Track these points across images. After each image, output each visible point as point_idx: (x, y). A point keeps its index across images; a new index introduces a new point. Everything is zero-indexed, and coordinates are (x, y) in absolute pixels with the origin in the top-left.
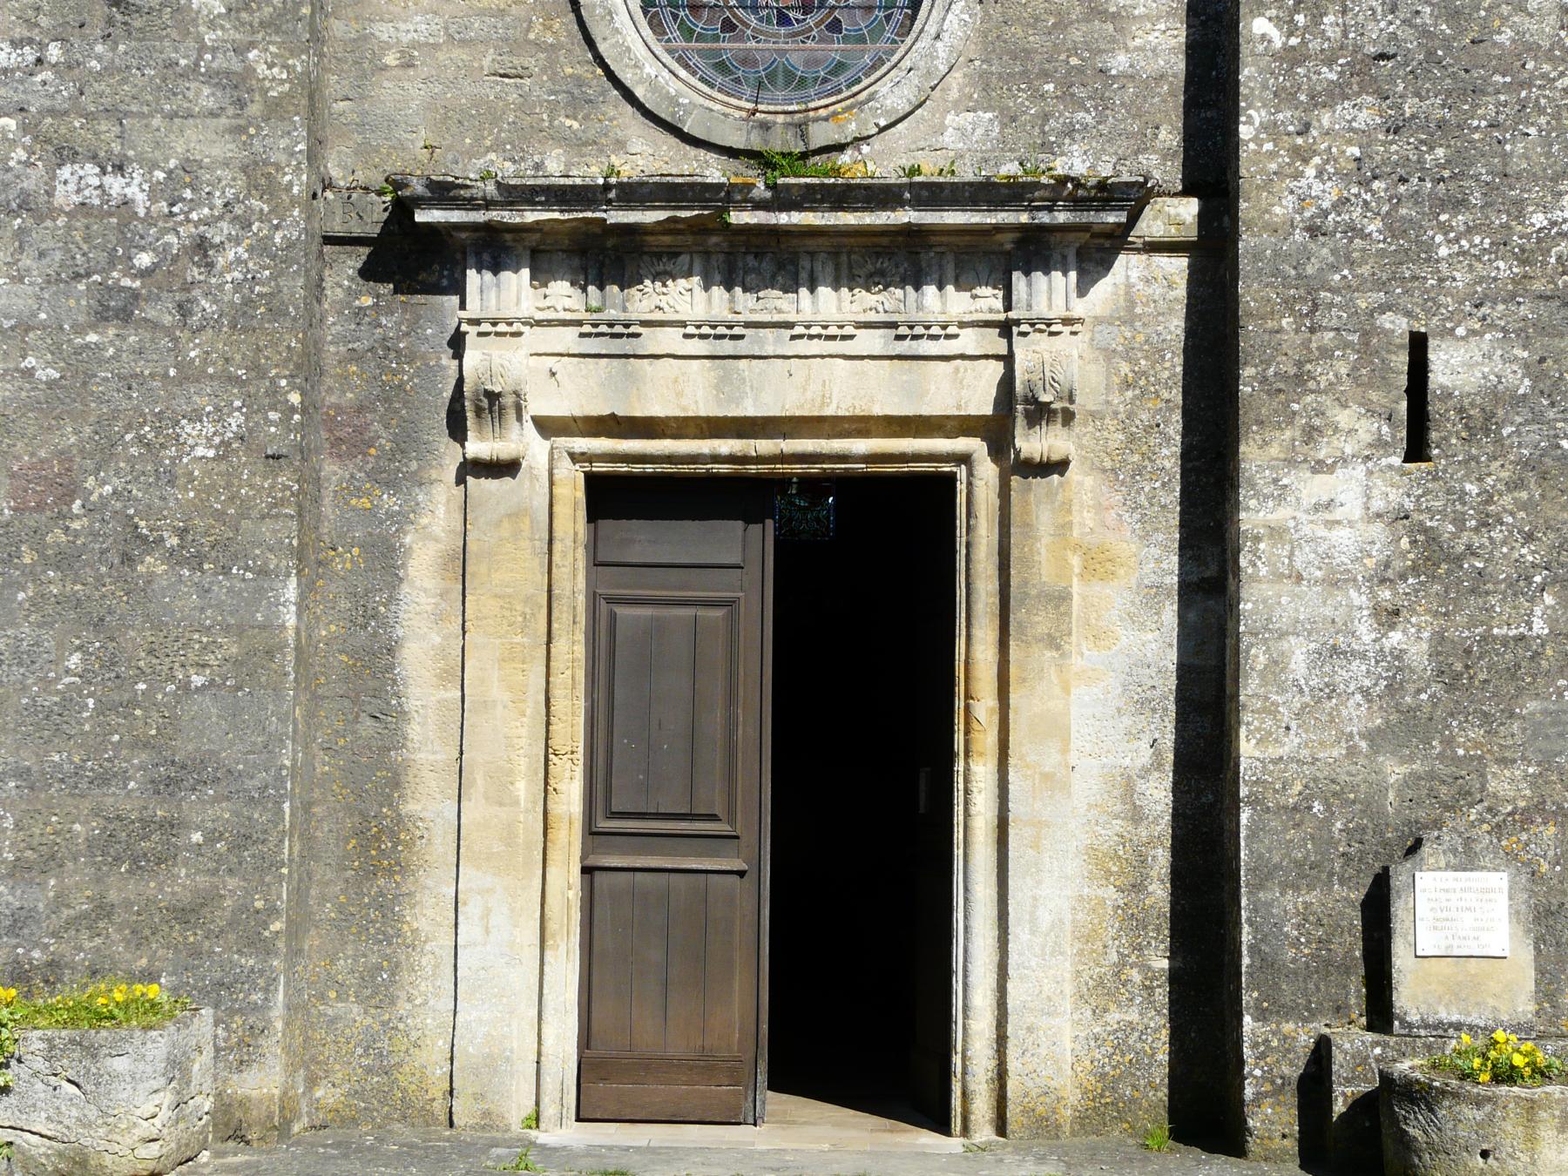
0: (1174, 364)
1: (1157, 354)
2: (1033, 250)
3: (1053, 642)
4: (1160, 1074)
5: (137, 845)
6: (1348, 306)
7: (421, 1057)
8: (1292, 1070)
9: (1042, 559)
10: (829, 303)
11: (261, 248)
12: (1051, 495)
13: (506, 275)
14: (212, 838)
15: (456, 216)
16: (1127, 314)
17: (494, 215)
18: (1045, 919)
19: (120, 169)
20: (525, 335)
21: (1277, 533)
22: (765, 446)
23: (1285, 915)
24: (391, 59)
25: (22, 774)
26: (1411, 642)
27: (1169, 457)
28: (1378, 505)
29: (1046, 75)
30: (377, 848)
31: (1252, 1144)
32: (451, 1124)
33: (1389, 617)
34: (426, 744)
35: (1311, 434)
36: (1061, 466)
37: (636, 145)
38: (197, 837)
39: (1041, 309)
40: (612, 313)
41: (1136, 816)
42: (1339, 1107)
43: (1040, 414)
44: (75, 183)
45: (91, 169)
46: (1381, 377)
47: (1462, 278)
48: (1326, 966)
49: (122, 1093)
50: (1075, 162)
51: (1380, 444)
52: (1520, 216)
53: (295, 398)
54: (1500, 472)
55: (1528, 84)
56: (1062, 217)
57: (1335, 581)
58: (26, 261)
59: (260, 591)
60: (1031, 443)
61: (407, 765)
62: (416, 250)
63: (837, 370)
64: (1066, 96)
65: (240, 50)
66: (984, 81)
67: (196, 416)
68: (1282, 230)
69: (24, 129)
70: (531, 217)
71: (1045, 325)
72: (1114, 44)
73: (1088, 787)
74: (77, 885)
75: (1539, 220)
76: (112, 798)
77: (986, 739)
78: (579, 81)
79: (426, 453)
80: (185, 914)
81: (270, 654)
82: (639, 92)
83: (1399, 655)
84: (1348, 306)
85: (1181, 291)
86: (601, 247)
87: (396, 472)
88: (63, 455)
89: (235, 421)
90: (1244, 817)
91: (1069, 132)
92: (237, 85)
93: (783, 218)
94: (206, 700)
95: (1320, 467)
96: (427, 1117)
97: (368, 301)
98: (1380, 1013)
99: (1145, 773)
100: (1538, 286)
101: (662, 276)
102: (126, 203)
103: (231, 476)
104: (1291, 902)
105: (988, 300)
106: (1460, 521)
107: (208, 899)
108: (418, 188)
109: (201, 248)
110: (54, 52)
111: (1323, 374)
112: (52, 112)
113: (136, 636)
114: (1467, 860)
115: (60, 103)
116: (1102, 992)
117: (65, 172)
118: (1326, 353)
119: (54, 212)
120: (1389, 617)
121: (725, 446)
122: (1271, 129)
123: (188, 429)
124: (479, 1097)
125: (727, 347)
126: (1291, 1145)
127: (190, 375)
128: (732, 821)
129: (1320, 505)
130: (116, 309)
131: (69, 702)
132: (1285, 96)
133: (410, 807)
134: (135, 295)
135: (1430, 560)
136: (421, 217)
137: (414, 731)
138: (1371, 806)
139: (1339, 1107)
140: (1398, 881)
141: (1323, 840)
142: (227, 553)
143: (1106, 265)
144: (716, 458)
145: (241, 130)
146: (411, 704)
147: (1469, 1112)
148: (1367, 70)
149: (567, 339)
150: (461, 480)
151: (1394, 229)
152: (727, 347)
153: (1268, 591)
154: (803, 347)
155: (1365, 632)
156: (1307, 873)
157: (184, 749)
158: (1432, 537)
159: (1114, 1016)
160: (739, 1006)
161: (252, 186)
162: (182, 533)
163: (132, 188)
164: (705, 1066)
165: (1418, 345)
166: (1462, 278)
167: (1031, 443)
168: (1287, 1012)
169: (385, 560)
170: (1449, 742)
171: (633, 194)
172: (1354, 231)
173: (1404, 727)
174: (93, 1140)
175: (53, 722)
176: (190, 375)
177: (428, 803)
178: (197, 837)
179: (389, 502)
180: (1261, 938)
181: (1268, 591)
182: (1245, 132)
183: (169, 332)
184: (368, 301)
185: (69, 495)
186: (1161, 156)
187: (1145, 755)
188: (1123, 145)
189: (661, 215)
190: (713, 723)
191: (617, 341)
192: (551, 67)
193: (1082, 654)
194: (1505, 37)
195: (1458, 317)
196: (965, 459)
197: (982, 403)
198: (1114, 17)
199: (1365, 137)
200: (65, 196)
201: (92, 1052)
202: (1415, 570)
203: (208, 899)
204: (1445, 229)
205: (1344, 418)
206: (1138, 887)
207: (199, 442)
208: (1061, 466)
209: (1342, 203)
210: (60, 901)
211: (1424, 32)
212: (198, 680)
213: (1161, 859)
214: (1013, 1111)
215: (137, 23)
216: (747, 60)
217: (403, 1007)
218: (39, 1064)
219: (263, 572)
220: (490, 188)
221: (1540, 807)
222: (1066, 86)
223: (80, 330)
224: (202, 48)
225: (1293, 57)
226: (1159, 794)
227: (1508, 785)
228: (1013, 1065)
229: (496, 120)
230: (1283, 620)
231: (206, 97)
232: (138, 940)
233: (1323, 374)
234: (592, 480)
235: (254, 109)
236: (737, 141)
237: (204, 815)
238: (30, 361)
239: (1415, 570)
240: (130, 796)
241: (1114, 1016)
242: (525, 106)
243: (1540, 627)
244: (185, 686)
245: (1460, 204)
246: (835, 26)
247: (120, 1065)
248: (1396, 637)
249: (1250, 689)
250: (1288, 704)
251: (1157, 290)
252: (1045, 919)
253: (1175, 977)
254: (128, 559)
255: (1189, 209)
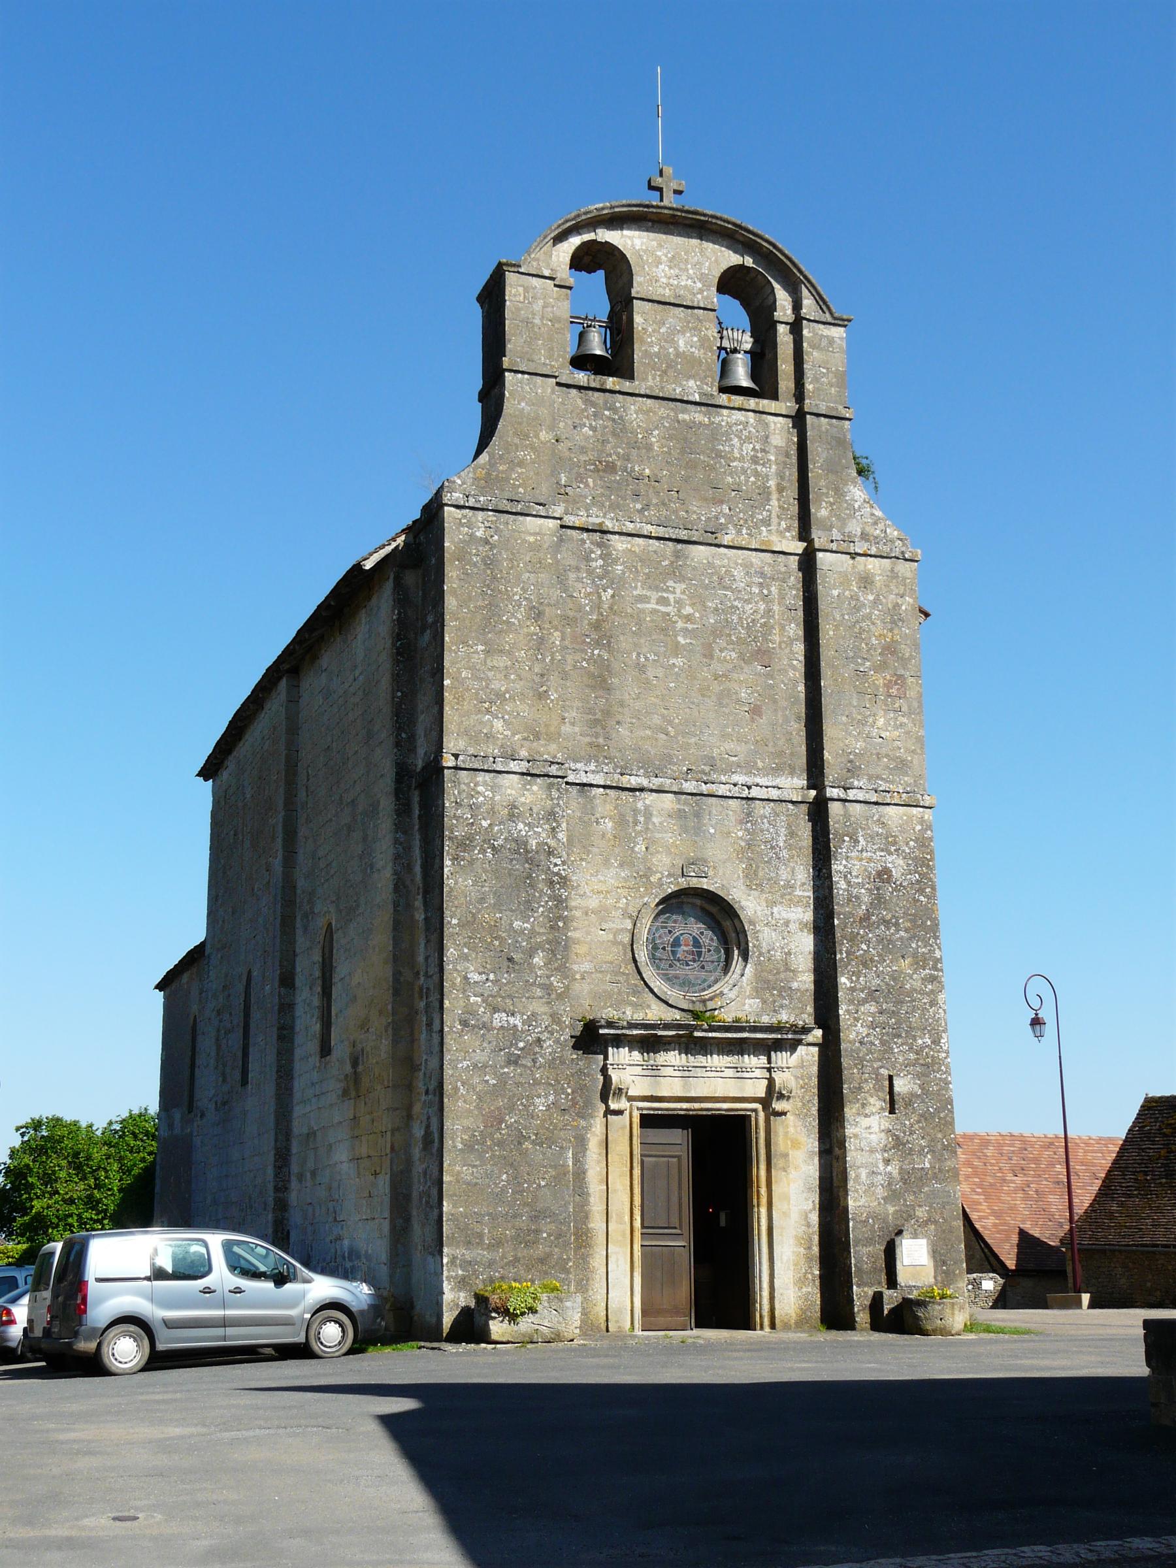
0: (815, 1081)
1: (810, 1078)
2: (778, 1046)
3: (784, 1170)
4: (818, 1308)
5: (527, 1238)
6: (871, 1066)
7: (597, 1309)
8: (867, 1303)
9: (780, 1143)
10: (716, 1060)
11: (557, 1041)
12: (783, 1122)
13: (621, 1049)
14: (549, 1235)
15: (612, 1032)
16: (801, 1065)
17: (624, 1031)
18: (785, 1258)
19: (513, 1015)
20: (626, 1067)
21: (856, 1136)
22: (697, 1105)
23: (863, 1255)
24: (578, 976)
25: (489, 1214)
26: (893, 1169)
27: (814, 1110)
28: (883, 1127)
29: (774, 989)
30: (583, 1239)
31: (857, 1326)
32: (607, 1331)
33: (887, 1162)
34: (596, 1206)
35: (863, 1105)
36: (785, 1114)
37: (654, 1006)
38: (545, 1235)
39: (779, 1064)
40: (652, 1062)
41: (808, 1225)
42: (886, 1312)
43: (781, 1096)
44: (499, 1019)
45: (504, 1015)
46: (881, 1089)
47: (901, 1059)
48: (875, 1270)
49: (570, 1313)
50: (784, 1017)
51: (882, 1109)
52: (915, 1040)
53: (569, 1091)
54: (914, 1118)
55: (914, 1001)
56: (790, 1036)
57: (872, 1151)
58: (485, 1045)
59: (561, 1154)
60: (778, 1106)
61: (590, 1211)
62: (591, 1039)
63: (721, 1082)
64: (780, 995)
65: (548, 977)
66: (756, 990)
67: (539, 1096)
68: (853, 1042)
69: (483, 1001)
70: (635, 1032)
71: (781, 1069)
72: (793, 979)
73: (795, 1216)
74: (507, 1252)
75: (920, 1042)
76: (518, 1222)
77: (764, 1200)
78: (636, 985)
79: (593, 1106)
80: (542, 1261)
81: (565, 1175)
82: (656, 990)
83: (890, 1174)
84: (871, 1066)
85: (816, 1058)
86: (650, 1042)
87: (584, 1114)
88: (499, 1109)
89: (551, 1098)
90: (851, 1224)
91: (782, 1006)
92: (548, 988)
93: (710, 1035)
94: (546, 1190)
95: (866, 1116)
96: (598, 1328)
97: (575, 1056)
98: (892, 1283)
99: (811, 1211)
100: (921, 1062)
101: (666, 1050)
102: (515, 1026)
103: (551, 1116)
104: (865, 1250)
105: (763, 1060)
106: (904, 1133)
107: (549, 1255)
108: (603, 1022)
109: (539, 1040)
110: (492, 977)
111: (866, 1087)
112: (492, 996)
113: (524, 1169)
114: (915, 1236)
115: (494, 993)
116: (801, 1282)
117: (496, 1016)
118: (866, 1081)
119: (493, 1029)
120: (887, 1162)
121: (685, 1105)
122: (848, 1011)
123: (537, 1100)
124: (617, 1322)
125: (687, 1074)
126: (868, 1326)
127: (537, 1083)
128: (681, 1229)
129: (867, 1128)
130: (513, 1061)
131: (504, 1190)
132: (851, 1002)
133: (591, 1225)
134: (519, 1056)
135: (898, 1144)
136: (601, 1031)
137: (592, 1200)
138: (885, 1220)
139: (886, 1312)
140: (897, 1243)
141: (873, 1231)
142: (551, 1141)
143: (795, 1049)
144: (681, 1110)
145: (550, 1003)
146: (591, 1191)
147: (937, 1307)
148: (872, 995)
149: (638, 1070)
150: (605, 1116)
151: (883, 1043)
152: (687, 1074)
153: (854, 1154)
154: (709, 1074)
155: (881, 1166)
156: (869, 1241)
157: (540, 1206)
158: (898, 1138)
159: (804, 1290)
160: (684, 1290)
161: (553, 1021)
162: (536, 1135)
163: (516, 1021)
164: (676, 1311)
165: (891, 1078)
166: (901, 1059)
167: (778, 1106)
168: (866, 1284)
169: (581, 1143)
170: (905, 1200)
171: (667, 1027)
172: (872, 1043)
173: (893, 1196)
174: (561, 1327)
175: (499, 1197)
176: (537, 1083)
177: (597, 1224)
178: (545, 1235)
179: (583, 1123)
180: (857, 1262)
181: (854, 1154)
182: (841, 1012)
183: (529, 1068)
184: (575, 1056)
185: (500, 1123)
186: (807, 1017)
187: (811, 1206)
188: (797, 1011)
189: (674, 1033)
190: (675, 1199)
191: (654, 1071)
192: (627, 981)
193: (793, 1174)
194: (908, 986)
195: (901, 1070)
196: (755, 1110)
197: (761, 1092)
198: (793, 971)
199: (873, 1015)
200: (496, 1023)
201: (561, 1300)
202: (894, 1148)
203: (549, 1255)
204: (896, 1043)
205: (872, 1100)
206: (809, 1248)
207: (540, 1105)
208: (785, 1114)
209: (868, 1035)
210: (503, 1257)
211: (887, 984)
212: (543, 1183)
213: (816, 1238)
214: (777, 1321)
215: (517, 967)
216: (677, 977)
217: (590, 1293)
218: (546, 1304)
219: (561, 1148)
220: (625, 1023)
221: (929, 1220)
222: (780, 992)
223: (502, 1067)
224: (537, 976)
225: (852, 989)
226: (814, 1218)
227: (921, 1213)
228: (777, 1306)
229: (611, 997)
230: (858, 1163)
231: (539, 992)
232: (529, 1270)
233: (866, 1087)
234: (641, 1115)
235: (553, 996)
236: (685, 1007)
237: (547, 1229)
238: (487, 1078)
239: (894, 1148)
240: (523, 1221)
241: (804, 1290)
242: (619, 993)
243: (927, 1165)
244: (539, 1185)
245: (899, 1036)
246: (703, 967)
247: (568, 1304)
248: (889, 1168)
249: (851, 1184)
250: (861, 1189)
251: (810, 1058)
252: (785, 1258)
253: (821, 1277)
254: (520, 1143)
255: (818, 1033)
